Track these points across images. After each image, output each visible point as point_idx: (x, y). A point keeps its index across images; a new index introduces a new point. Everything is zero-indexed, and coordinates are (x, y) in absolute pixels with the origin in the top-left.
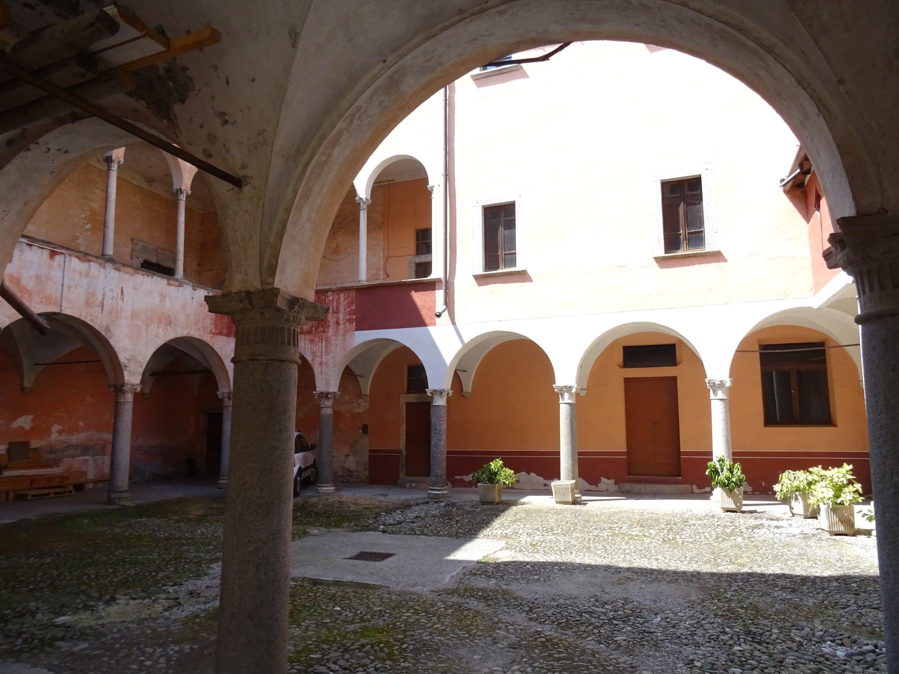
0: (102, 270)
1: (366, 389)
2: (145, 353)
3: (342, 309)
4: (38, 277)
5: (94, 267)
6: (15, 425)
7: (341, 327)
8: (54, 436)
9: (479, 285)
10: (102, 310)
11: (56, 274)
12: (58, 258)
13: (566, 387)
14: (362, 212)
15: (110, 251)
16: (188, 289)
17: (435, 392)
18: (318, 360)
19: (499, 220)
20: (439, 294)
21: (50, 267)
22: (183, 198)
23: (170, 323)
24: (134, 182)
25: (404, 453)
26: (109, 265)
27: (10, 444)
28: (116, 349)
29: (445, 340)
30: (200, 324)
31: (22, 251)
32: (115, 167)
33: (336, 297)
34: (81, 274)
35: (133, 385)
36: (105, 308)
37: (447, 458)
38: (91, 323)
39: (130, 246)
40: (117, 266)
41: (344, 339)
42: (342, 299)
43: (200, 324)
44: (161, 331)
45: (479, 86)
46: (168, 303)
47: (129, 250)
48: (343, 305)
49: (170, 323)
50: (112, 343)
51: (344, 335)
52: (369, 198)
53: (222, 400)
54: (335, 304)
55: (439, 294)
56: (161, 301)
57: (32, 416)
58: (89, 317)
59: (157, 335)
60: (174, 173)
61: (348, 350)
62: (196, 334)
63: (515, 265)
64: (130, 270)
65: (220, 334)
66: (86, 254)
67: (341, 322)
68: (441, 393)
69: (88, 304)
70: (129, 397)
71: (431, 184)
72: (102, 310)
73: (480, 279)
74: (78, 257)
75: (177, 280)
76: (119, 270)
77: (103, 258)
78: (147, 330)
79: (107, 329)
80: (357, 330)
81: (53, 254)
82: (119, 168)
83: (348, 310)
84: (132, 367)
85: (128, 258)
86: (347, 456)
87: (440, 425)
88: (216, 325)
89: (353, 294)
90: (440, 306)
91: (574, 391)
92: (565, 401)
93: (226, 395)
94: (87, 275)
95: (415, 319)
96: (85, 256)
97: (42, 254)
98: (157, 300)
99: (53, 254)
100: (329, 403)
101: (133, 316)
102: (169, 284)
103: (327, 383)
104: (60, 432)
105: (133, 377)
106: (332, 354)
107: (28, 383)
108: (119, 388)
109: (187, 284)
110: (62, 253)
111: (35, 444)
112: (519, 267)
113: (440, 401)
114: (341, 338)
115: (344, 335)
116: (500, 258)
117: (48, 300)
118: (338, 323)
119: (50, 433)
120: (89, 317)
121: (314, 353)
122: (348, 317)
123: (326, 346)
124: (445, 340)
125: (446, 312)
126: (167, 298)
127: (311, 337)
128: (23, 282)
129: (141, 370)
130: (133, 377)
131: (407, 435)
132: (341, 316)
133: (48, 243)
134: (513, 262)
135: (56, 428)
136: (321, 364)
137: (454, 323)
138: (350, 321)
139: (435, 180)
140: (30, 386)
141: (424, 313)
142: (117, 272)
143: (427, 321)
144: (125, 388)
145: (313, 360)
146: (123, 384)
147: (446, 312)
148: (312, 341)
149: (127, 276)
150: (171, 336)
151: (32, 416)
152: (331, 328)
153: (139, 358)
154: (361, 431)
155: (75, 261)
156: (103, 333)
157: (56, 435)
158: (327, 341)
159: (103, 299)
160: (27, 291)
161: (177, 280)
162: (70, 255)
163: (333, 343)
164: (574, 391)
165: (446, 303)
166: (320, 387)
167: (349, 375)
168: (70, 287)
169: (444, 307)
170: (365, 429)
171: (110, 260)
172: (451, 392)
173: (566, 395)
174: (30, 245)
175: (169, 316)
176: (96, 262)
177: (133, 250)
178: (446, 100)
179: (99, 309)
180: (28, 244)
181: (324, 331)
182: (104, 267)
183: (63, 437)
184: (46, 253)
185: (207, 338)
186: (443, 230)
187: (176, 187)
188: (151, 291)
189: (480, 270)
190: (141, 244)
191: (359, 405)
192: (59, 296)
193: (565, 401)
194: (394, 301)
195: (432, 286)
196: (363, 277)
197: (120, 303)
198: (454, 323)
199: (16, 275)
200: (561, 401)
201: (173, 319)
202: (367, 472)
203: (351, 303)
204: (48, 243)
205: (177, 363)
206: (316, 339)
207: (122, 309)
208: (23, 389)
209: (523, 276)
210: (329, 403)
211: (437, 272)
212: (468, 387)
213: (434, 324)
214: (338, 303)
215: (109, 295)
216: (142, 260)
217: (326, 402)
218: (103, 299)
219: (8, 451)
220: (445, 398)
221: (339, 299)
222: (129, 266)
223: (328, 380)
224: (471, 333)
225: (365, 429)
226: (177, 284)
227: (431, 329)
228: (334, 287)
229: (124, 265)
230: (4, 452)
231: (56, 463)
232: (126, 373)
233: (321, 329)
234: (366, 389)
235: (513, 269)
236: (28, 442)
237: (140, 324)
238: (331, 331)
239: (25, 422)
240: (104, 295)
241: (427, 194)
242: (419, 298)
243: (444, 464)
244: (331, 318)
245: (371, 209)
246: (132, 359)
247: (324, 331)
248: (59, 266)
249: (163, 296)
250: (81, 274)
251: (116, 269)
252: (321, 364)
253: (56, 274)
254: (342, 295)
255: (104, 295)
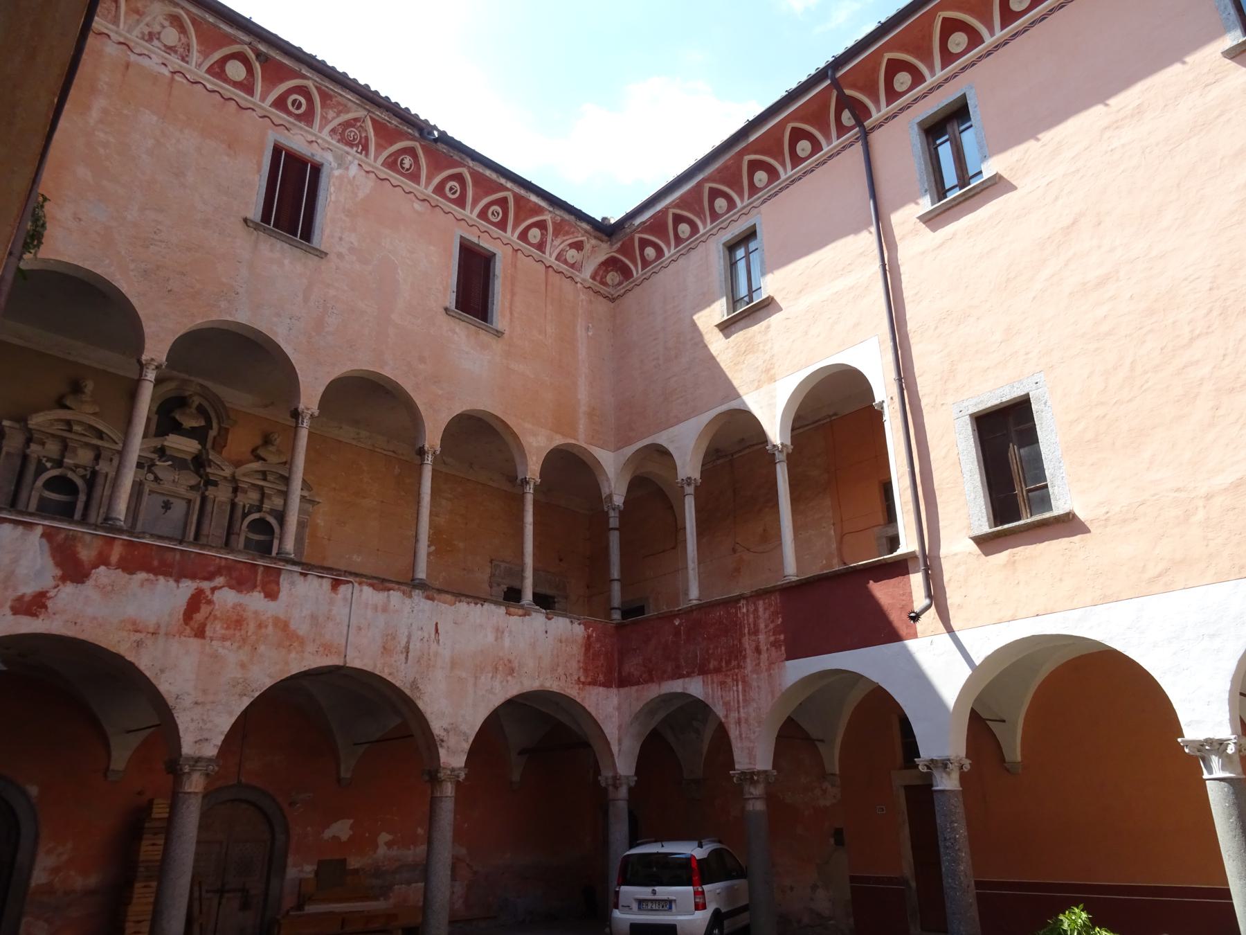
0: (407, 601)
1: (834, 764)
2: (473, 719)
3: (762, 626)
4: (313, 617)
5: (395, 597)
6: (328, 834)
7: (764, 656)
8: (382, 851)
9: (987, 554)
10: (407, 658)
11: (340, 611)
12: (343, 589)
13: (1210, 741)
14: (778, 466)
15: (421, 574)
16: (538, 619)
17: (932, 763)
18: (734, 715)
19: (1006, 434)
20: (916, 580)
21: (331, 602)
22: (530, 490)
23: (512, 671)
24: (491, 483)
25: (913, 884)
26: (417, 594)
27: (321, 864)
28: (428, 716)
29: (942, 662)
30: (560, 670)
31: (293, 583)
32: (429, 459)
33: (752, 608)
34: (375, 608)
35: (453, 770)
36: (410, 655)
37: (979, 897)
38: (389, 679)
39: (488, 570)
40: (430, 593)
41: (770, 675)
42: (761, 610)
43: (560, 670)
44: (497, 684)
45: (934, 230)
46: (507, 642)
47: (486, 577)
48: (762, 622)
49: (512, 671)
50: (421, 705)
51: (769, 669)
52: (788, 442)
53: (606, 790)
54: (751, 620)
55: (916, 580)
56: (496, 639)
57: (352, 821)
58: (386, 670)
59: (491, 691)
60: (518, 460)
61: (778, 695)
62: (553, 686)
63: (1050, 509)
64: (449, 597)
65: (594, 683)
66: (384, 580)
67: (763, 647)
68: (944, 764)
69: (386, 650)
70: (449, 789)
71: (878, 399)
72: (407, 658)
73: (986, 543)
74: (371, 585)
75: (522, 607)
76: (432, 599)
77: (411, 584)
78: (475, 685)
79: (414, 685)
80: (788, 659)
81: (336, 584)
82: (535, 490)
83: (772, 626)
84: (452, 741)
85: (486, 586)
86: (814, 888)
87: (955, 829)
88: (586, 670)
89: (776, 599)
90: (919, 599)
91: (1231, 749)
92: (195, 784)
93: (610, 782)
94: (385, 609)
95: (883, 630)
96: (381, 583)
97: (321, 585)
98: (491, 638)
99: (336, 584)
100: (758, 791)
101: (454, 664)
102: (508, 613)
103: (751, 755)
104: (389, 845)
105: (453, 757)
106: (754, 703)
107: (345, 773)
108: (433, 775)
109: (536, 611)
110: (348, 582)
111: (354, 863)
112: (1059, 507)
113: (947, 783)
114: (765, 675)
115: (769, 669)
116: (1020, 500)
117: (327, 648)
118: (758, 650)
119: (375, 846)
120: (386, 670)
121: (726, 704)
122: (772, 639)
123: (744, 691)
124: (942, 662)
125: (933, 609)
126: (506, 634)
127: (720, 677)
128: (293, 626)
129: (467, 746)
130: (453, 757)
131: (914, 848)
132: (762, 637)
133: (329, 570)
134: (1045, 503)
135: (384, 837)
136: (739, 722)
137: (950, 630)
138: (775, 644)
139: (884, 390)
140: (349, 776)
141: (897, 618)
142: (429, 602)
143: (903, 630)
144: (441, 775)
145: (726, 716)
146: (438, 768)
147: (933, 609)
148: (722, 684)
149: (444, 607)
150: (514, 690)
151: (352, 821)
152: (748, 660)
153: (464, 728)
154: (832, 841)
155: (367, 590)
156: (407, 692)
157: (384, 850)
158: (744, 682)
159: (408, 642)
160: (298, 637)
161: (522, 607)
162: (360, 584)
163: (755, 684)
164: (1231, 749)
165: (929, 595)
166: (742, 762)
167: (793, 736)
168: (360, 629)
169: (927, 601)
170: (838, 835)
171: (422, 586)
172: (967, 764)
173: (1215, 761)
174: (305, 575)
175: (510, 661)
176: (399, 589)
177: (492, 575)
178: (884, 265)
179: (403, 657)
180: (301, 574)
181: (739, 667)
182: (410, 597)
183: (394, 852)
184: (326, 584)
185: (573, 692)
186: (906, 469)
187: (520, 477)
188: (481, 626)
189: (984, 526)
190: (503, 565)
191: (825, 791)
192: (343, 642)
193: (1215, 771)
194: (849, 604)
195: (900, 568)
196: (791, 569)
197: (434, 646)
198: (950, 630)
199: (282, 616)
200: (1206, 775)
201: (516, 664)
202: (851, 920)
203: (775, 614)
204: (329, 570)
205: (536, 735)
206: (729, 680)
207: (436, 654)
208: (339, 780)
209: (1068, 525)
210: (758, 791)
211: (908, 544)
212: (1014, 751)
213: (915, 636)
214: (757, 618)
215: (417, 635)
216: (504, 587)
217: (752, 790)
218: (408, 642)
219: (317, 873)
220: (955, 776)
221: (756, 610)
222: (447, 592)
223: (754, 752)
224: (986, 641)
225: (838, 835)
226: (521, 612)
227: (911, 644)
228: (747, 592)
229: (440, 591)
230: (312, 876)
231: (384, 892)
232: (442, 752)
233: (734, 663)
234: (834, 764)
235: (1047, 515)
236: (345, 860)
237: (464, 675)
238: (749, 665)
239: (341, 829)
240: (409, 637)
241: (875, 417)
242: (882, 591)
243: (974, 912)
244: (747, 643)
245: (792, 460)
246: (452, 729)
247: (739, 667)
248: (345, 599)
249: (499, 632)
250: (375, 608)
251: (428, 598)
252: (739, 722)
253: (340, 611)
254: (761, 602)
255: (409, 637)
